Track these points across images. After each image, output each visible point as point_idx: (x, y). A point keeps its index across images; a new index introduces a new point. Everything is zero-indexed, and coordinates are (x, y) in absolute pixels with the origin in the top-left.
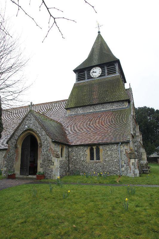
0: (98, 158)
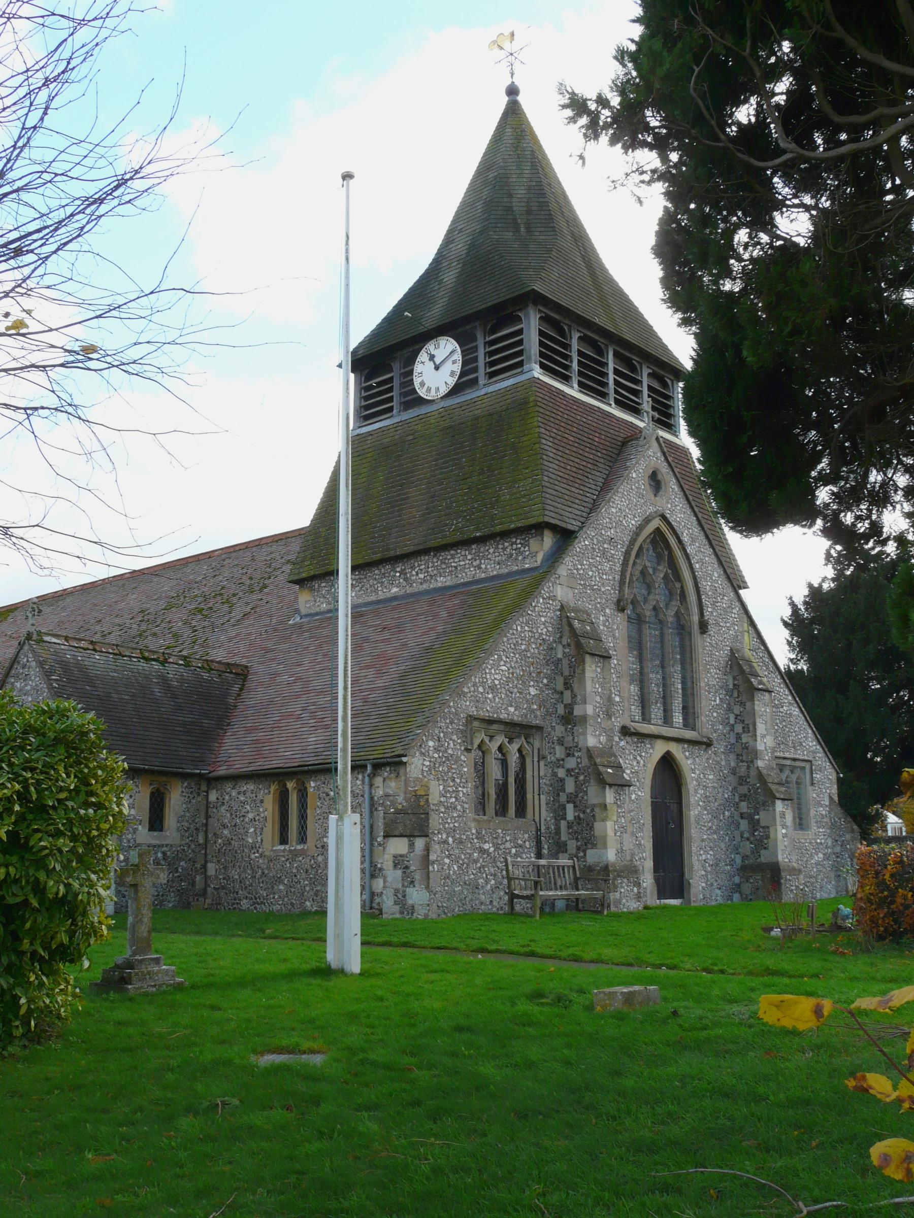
0: (303, 839)
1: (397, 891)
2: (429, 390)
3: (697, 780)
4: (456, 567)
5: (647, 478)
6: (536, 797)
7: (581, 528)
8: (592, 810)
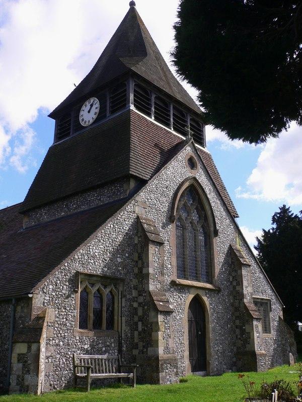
1: (18, 376)
2: (85, 122)
3: (213, 309)
4: (90, 201)
5: (187, 161)
6: (120, 318)
7: (150, 179)
8: (151, 325)
